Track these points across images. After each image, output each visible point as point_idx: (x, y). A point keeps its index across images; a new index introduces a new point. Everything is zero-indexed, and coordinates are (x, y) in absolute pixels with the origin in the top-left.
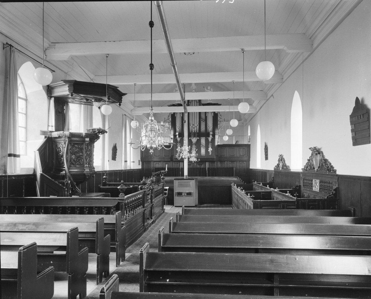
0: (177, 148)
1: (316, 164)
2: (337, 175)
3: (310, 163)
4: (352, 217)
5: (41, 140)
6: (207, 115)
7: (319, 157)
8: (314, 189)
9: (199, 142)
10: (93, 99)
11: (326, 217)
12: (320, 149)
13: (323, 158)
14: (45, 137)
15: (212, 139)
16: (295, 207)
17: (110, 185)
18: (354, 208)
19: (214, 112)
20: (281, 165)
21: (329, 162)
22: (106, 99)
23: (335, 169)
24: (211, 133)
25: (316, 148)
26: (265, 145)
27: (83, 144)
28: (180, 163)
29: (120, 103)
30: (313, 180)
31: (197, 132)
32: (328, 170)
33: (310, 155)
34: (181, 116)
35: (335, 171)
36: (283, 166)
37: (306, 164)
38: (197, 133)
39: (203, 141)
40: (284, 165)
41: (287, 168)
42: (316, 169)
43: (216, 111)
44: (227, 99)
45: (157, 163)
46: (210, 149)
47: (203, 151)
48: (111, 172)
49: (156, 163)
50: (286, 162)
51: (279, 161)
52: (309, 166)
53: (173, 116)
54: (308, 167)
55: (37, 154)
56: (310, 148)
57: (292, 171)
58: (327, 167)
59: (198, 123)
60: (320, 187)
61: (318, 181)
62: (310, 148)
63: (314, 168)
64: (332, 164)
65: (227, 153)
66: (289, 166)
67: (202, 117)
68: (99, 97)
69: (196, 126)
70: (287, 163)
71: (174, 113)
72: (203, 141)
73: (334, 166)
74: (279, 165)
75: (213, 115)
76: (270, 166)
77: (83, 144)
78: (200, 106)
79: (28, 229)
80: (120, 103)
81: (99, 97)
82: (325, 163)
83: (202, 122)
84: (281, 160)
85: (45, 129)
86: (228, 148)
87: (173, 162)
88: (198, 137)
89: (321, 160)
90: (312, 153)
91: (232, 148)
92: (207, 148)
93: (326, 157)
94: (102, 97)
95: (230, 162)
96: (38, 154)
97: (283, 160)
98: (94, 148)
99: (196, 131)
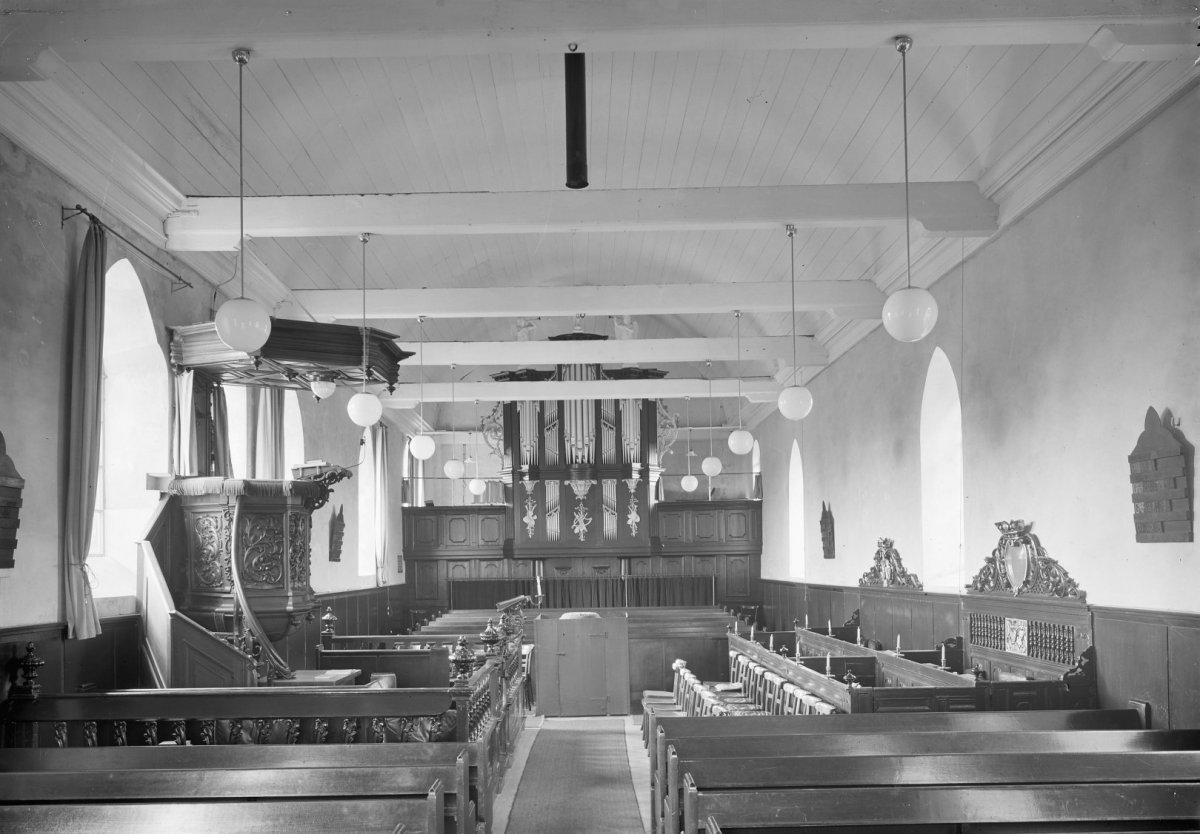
0: (524, 513)
1: (1015, 570)
2: (1089, 608)
3: (995, 569)
4: (1140, 728)
5: (151, 508)
6: (621, 406)
7: (1023, 552)
8: (1010, 648)
9: (595, 493)
10: (310, 373)
11: (1054, 732)
12: (1028, 528)
13: (1039, 554)
14: (163, 495)
15: (639, 484)
16: (973, 707)
17: (342, 643)
18: (1147, 704)
19: (646, 402)
20: (886, 570)
21: (1060, 568)
22: (358, 372)
23: (1080, 588)
24: (637, 466)
25: (1021, 524)
26: (822, 510)
27: (279, 515)
28: (534, 564)
29: (391, 384)
30: (1007, 622)
31: (589, 461)
32: (1057, 591)
33: (996, 545)
34: (538, 409)
35: (1083, 596)
36: (893, 573)
37: (981, 571)
38: (591, 466)
39: (609, 489)
40: (898, 573)
41: (909, 581)
42: (1015, 589)
43: (651, 397)
44: (704, 363)
45: (459, 563)
46: (633, 518)
47: (610, 525)
48: (341, 597)
49: (455, 563)
50: (903, 562)
51: (878, 558)
52: (991, 574)
53: (511, 411)
54: (987, 582)
55: (147, 547)
56: (999, 525)
57: (926, 589)
58: (1053, 583)
59: (591, 434)
60: (1029, 642)
61: (1022, 624)
62: (999, 525)
63: (1009, 585)
64: (1070, 576)
65: (687, 528)
66: (916, 577)
67: (606, 416)
68: (336, 368)
69: (586, 442)
70: (909, 567)
71: (513, 404)
72: (609, 489)
73: (1076, 581)
74: (880, 570)
75: (641, 407)
76: (848, 571)
77: (279, 515)
78: (598, 378)
79: (295, 789)
80: (391, 384)
81: (336, 368)
82: (1044, 569)
83: (604, 429)
84: (888, 557)
85: (161, 469)
86: (734, 517)
87: (513, 562)
88: (593, 477)
89: (1032, 562)
90: (1002, 539)
91: (707, 512)
92: (622, 513)
93: (1051, 554)
94: (341, 368)
95: (698, 559)
96: (151, 548)
97: (893, 555)
98: (311, 527)
99: (586, 460)
